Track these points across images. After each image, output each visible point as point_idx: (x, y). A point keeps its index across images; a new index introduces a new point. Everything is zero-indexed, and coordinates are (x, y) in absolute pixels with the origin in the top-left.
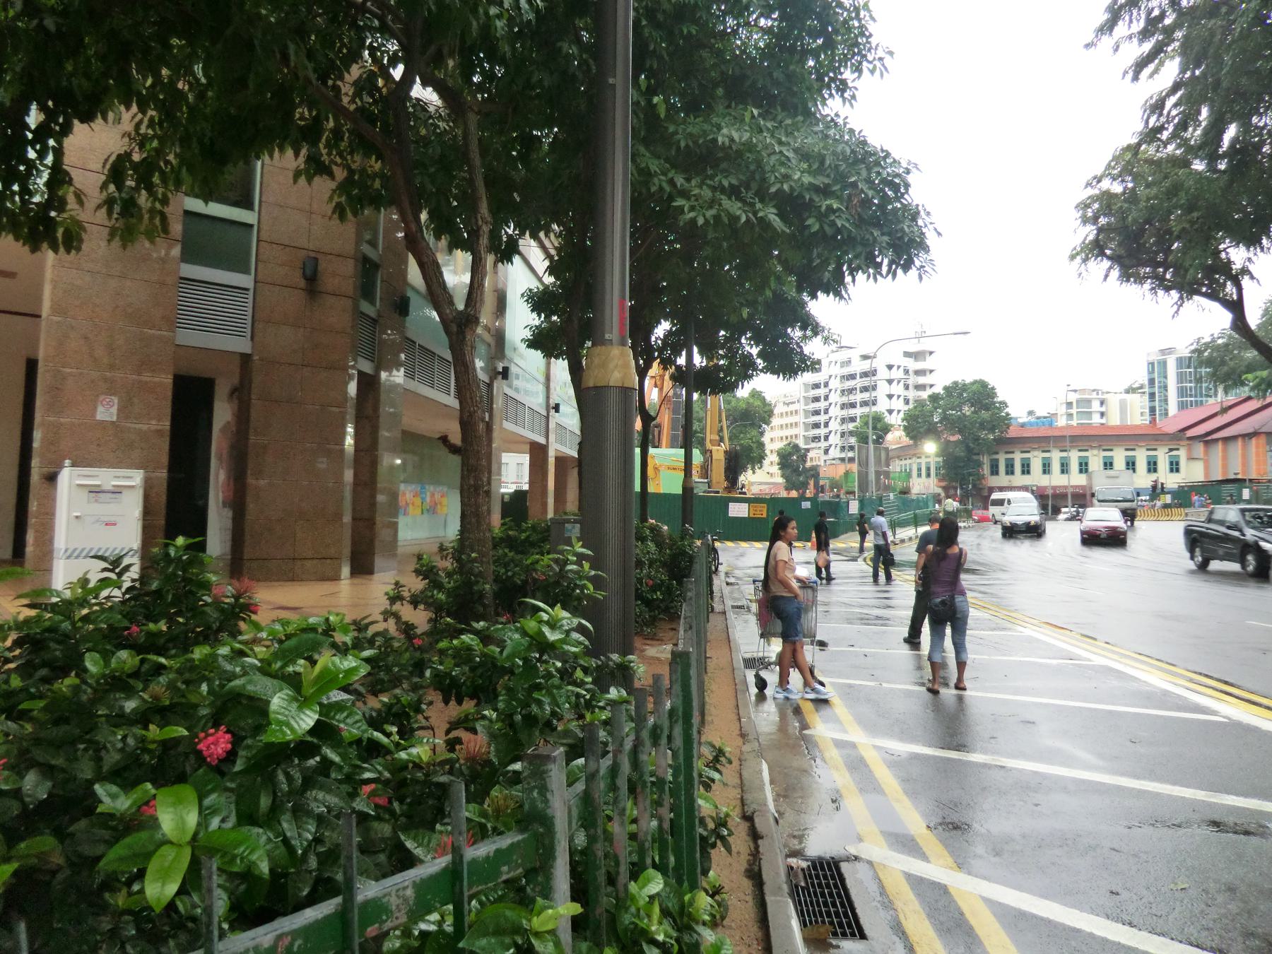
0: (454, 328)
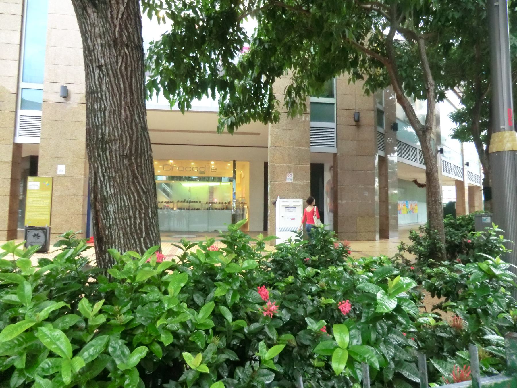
0: (421, 133)
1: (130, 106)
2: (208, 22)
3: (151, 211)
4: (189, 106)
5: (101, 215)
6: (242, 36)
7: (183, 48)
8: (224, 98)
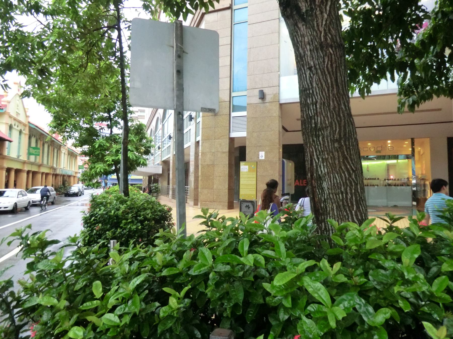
1: (336, 97)
2: (384, 10)
3: (360, 187)
4: (369, 91)
5: (317, 190)
6: (421, 14)
7: (361, 40)
8: (404, 78)
